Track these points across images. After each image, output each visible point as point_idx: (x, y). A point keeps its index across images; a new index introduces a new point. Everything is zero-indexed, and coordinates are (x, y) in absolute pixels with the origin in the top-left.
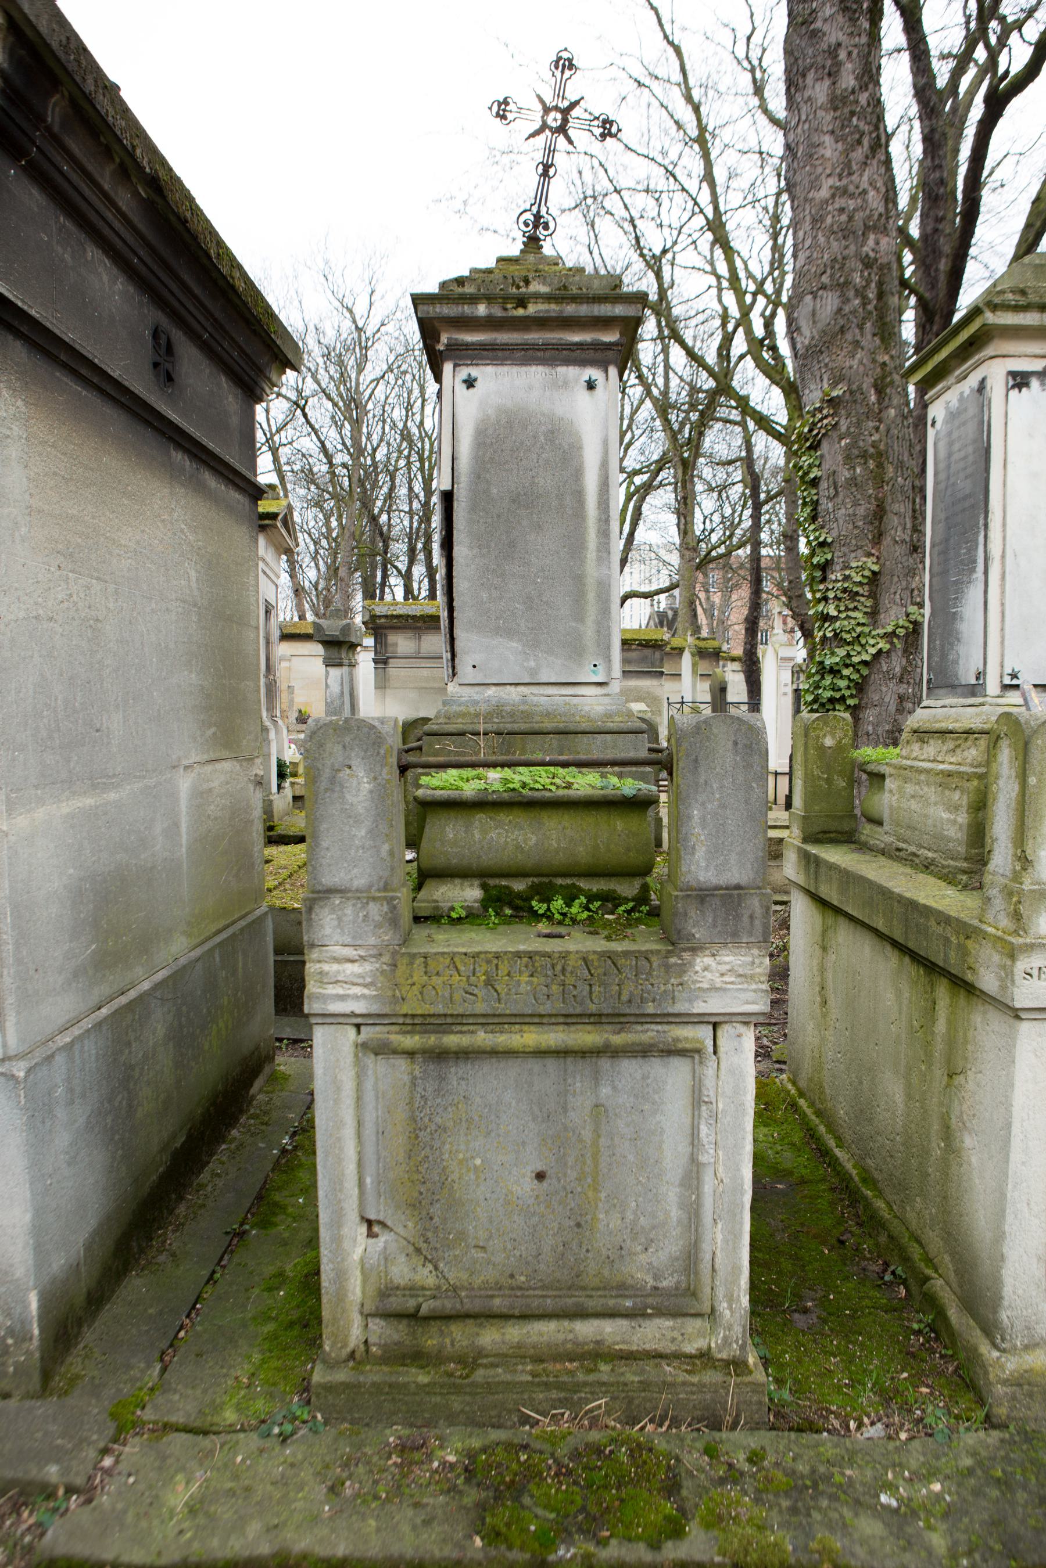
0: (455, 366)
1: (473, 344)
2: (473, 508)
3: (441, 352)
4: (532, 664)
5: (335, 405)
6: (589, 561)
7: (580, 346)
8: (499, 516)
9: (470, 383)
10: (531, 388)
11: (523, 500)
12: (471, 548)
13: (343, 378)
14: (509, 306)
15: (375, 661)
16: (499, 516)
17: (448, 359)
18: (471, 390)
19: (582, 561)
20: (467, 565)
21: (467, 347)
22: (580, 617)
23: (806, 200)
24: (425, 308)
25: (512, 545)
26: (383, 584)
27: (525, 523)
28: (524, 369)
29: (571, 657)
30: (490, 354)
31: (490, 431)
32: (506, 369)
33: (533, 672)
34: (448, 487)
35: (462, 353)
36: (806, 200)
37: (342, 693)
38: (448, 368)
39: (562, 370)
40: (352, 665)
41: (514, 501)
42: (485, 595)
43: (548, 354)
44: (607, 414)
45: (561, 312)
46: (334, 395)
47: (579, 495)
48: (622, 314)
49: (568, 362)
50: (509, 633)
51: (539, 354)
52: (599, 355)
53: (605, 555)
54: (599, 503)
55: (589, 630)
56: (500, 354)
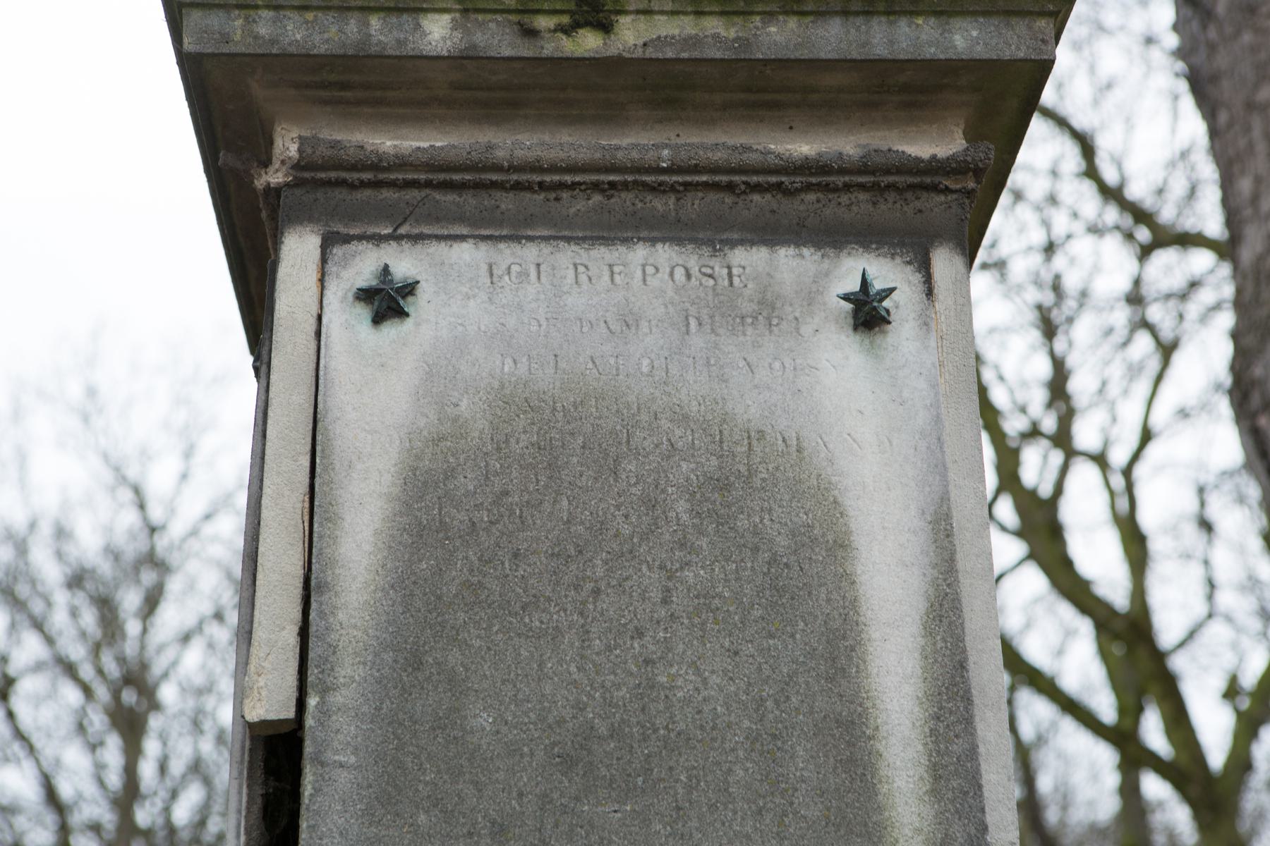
0: (328, 242)
1: (402, 163)
2: (388, 793)
3: (273, 193)
5: (87, 691)
7: (818, 175)
9: (386, 301)
10: (630, 321)
14: (544, 23)
17: (303, 217)
18: (391, 330)
21: (379, 174)
23: (1250, 106)
24: (215, 20)
28: (601, 255)
30: (469, 201)
31: (467, 481)
32: (530, 252)
34: (273, 704)
35: (353, 198)
36: (1250, 106)
38: (298, 250)
39: (750, 260)
41: (568, 763)
43: (695, 204)
44: (938, 420)
45: (745, 43)
46: (87, 672)
47: (850, 736)
48: (980, 52)
49: (769, 233)
51: (659, 204)
52: (889, 210)
56: (507, 202)
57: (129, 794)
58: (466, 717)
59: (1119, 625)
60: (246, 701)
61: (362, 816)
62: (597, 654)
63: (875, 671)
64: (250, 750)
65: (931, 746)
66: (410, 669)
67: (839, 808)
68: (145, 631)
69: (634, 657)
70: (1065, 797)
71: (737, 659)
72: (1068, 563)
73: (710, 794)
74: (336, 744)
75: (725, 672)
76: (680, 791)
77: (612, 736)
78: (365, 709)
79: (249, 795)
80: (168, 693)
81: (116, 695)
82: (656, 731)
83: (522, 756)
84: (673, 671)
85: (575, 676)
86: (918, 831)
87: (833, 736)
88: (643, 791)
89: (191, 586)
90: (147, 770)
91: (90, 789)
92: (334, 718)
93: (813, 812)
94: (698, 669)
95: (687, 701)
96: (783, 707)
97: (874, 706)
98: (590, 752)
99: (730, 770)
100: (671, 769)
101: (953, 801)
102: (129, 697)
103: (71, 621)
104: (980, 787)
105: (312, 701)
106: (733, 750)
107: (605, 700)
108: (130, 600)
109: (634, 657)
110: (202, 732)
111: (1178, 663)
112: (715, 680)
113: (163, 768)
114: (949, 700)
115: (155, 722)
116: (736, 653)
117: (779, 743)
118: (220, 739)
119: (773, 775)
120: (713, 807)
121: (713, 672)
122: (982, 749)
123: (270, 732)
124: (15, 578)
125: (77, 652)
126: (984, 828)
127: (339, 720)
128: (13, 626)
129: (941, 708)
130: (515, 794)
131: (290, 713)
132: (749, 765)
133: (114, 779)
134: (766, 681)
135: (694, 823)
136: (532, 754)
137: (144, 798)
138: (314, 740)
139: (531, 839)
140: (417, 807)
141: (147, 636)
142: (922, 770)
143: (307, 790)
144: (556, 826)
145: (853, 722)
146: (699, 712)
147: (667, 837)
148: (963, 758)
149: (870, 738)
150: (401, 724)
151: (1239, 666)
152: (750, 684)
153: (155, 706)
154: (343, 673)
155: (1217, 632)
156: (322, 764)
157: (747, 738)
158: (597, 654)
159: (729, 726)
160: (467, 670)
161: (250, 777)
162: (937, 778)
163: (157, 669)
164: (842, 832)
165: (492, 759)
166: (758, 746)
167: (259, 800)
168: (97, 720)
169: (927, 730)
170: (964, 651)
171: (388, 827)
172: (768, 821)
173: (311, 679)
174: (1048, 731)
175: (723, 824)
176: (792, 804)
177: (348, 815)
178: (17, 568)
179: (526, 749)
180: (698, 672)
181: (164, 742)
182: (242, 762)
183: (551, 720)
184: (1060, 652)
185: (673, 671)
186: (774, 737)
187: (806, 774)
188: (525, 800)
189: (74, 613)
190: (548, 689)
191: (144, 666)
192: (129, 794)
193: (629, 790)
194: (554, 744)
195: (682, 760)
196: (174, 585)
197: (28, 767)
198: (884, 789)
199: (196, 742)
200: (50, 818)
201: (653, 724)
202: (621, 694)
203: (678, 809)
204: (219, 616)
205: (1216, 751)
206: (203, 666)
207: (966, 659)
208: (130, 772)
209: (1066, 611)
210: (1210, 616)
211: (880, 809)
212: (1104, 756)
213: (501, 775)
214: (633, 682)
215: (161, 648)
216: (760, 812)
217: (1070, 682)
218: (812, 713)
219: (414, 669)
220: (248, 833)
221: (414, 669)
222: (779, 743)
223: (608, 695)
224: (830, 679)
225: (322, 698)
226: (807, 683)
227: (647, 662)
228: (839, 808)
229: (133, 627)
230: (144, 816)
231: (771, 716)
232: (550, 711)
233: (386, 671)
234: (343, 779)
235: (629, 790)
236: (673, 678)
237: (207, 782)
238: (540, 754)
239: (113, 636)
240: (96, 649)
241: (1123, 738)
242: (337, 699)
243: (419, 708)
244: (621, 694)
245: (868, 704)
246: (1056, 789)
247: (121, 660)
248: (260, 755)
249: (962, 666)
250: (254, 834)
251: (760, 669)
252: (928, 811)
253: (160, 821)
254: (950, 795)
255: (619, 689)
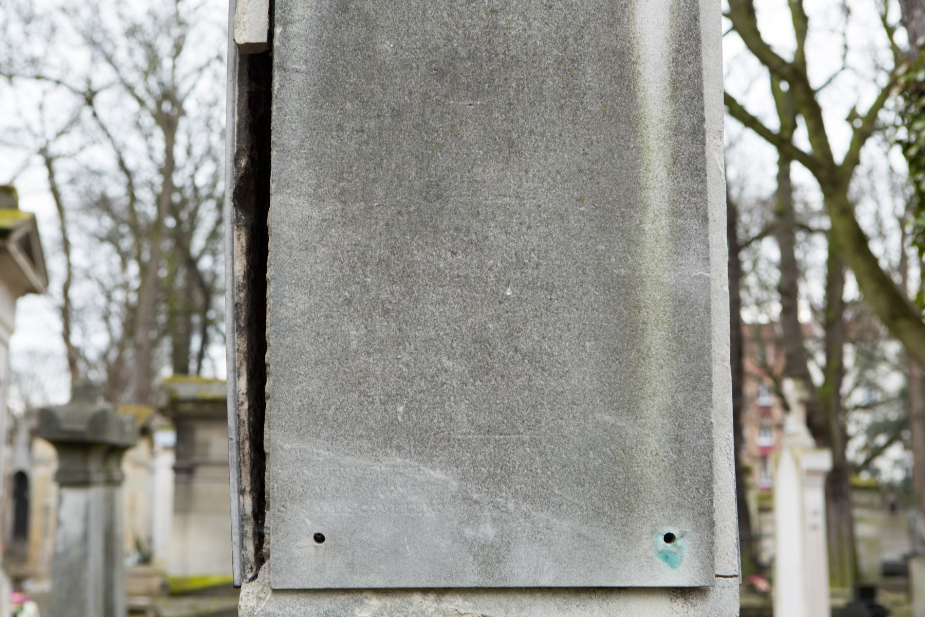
2: (327, 89)
4: (488, 531)
5: (141, 102)
6: (650, 241)
8: (397, 114)
11: (468, 72)
12: (317, 199)
13: (154, 62)
15: (177, 469)
16: (397, 114)
19: (631, 238)
20: (307, 248)
22: (624, 397)
25: (434, 191)
26: (201, 356)
27: (470, 133)
29: (598, 513)
33: (491, 554)
34: (254, 34)
37: (85, 537)
40: (113, 482)
41: (441, 74)
42: (354, 332)
46: (140, 91)
47: (620, 63)
50: (424, 441)
53: (694, 225)
54: (675, 85)
55: (652, 437)
57: (168, 167)
58: (376, 43)
59: (785, 71)
60: (236, 30)
61: (311, 103)
62: (461, 5)
63: (640, 21)
64: (240, 64)
65: (672, 69)
66: (340, 12)
67: (612, 106)
68: (174, 67)
69: (485, 8)
70: (743, 181)
71: (551, 11)
72: (757, 34)
73: (531, 95)
74: (293, 57)
75: (543, 19)
76: (512, 93)
77: (469, 58)
78: (311, 36)
79: (239, 91)
80: (189, 105)
81: (159, 104)
82: (497, 55)
83: (411, 69)
84: (510, 17)
85: (446, 19)
86: (662, 121)
87: (610, 61)
88: (488, 93)
89: (202, 38)
90: (179, 153)
91: (146, 164)
92: (292, 41)
93: (595, 108)
94: (525, 16)
95: (518, 37)
96: (579, 42)
97: (638, 42)
98: (455, 68)
99: (544, 81)
100: (506, 79)
101: (684, 103)
102: (167, 106)
103: (130, 57)
104: (702, 94)
105: (278, 30)
106: (546, 69)
107: (465, 35)
108: (164, 46)
109: (485, 8)
110: (211, 130)
111: (823, 99)
112: (536, 24)
113: (189, 152)
114: (686, 40)
115: (182, 123)
116: (550, 7)
117: (576, 65)
118: (223, 134)
119: (571, 85)
120: (532, 104)
121: (535, 19)
122: (704, 73)
123: (252, 52)
124: (93, 29)
125: (133, 78)
126: (702, 120)
127: (295, 43)
128: (93, 60)
129: (680, 45)
130: (407, 92)
131: (264, 39)
132: (556, 78)
133: (160, 156)
134: (569, 26)
135: (520, 113)
136: (418, 68)
137: (179, 169)
138: (280, 55)
139: (417, 120)
140: (345, 99)
141: (176, 70)
142: (666, 84)
143: (276, 85)
144: (433, 112)
145: (623, 53)
146: (525, 44)
147: (502, 121)
148: (693, 76)
149: (634, 63)
150: (334, 47)
151: (857, 102)
152: (558, 27)
153: (183, 113)
154: (297, 13)
155: (847, 77)
156: (285, 70)
157: (555, 61)
158: (461, 5)
159: (544, 53)
160: (377, 13)
161: (239, 80)
162: (675, 89)
163: (183, 89)
164: (613, 121)
165: (392, 70)
166: (562, 66)
167: (246, 95)
168: (148, 121)
169: (671, 59)
170: (698, 9)
171: (327, 110)
172: (566, 113)
173: (277, 16)
174: (736, 141)
175: (538, 114)
176: (582, 103)
177: (302, 102)
178: (93, 22)
179: (414, 65)
180: (525, 19)
181: (189, 135)
182: (234, 71)
183: (430, 47)
184: (746, 92)
185: (510, 17)
186: (573, 61)
187: (592, 84)
188: (413, 96)
189: (131, 52)
190: (429, 27)
191: (175, 88)
192: (168, 167)
193: (479, 92)
194: (432, 62)
195: (513, 74)
196: (192, 37)
197: (107, 144)
198: (641, 95)
199: (209, 136)
200: (123, 178)
201: (496, 51)
202: (475, 31)
203: (510, 104)
204: (219, 58)
205: (839, 153)
206: (211, 89)
207: (698, 14)
208: (169, 152)
209: (753, 61)
210: (843, 68)
211: (638, 107)
212: (770, 153)
213: (398, 81)
214: (483, 24)
215: (185, 77)
216: (562, 107)
217: (753, 109)
218: (597, 46)
219: (343, 12)
220: (239, 114)
221: (343, 12)
222: (576, 65)
223: (467, 32)
224: (610, 25)
225: (284, 28)
226: (595, 27)
227: (493, 11)
228: (612, 106)
229: (167, 63)
230: (178, 179)
231: (571, 48)
232: (430, 41)
233: (325, 13)
234: (298, 79)
235: (479, 92)
236: (509, 22)
237: (215, 160)
238: (423, 68)
239: (155, 69)
240: (146, 74)
241: (782, 142)
242: (294, 29)
243: (346, 37)
244: (475, 31)
245: (634, 41)
246: (738, 177)
247: (161, 84)
248: (246, 67)
249: (696, 18)
250: (243, 115)
251: (565, 18)
252: (668, 109)
253: (188, 183)
254: (683, 99)
255: (474, 28)
